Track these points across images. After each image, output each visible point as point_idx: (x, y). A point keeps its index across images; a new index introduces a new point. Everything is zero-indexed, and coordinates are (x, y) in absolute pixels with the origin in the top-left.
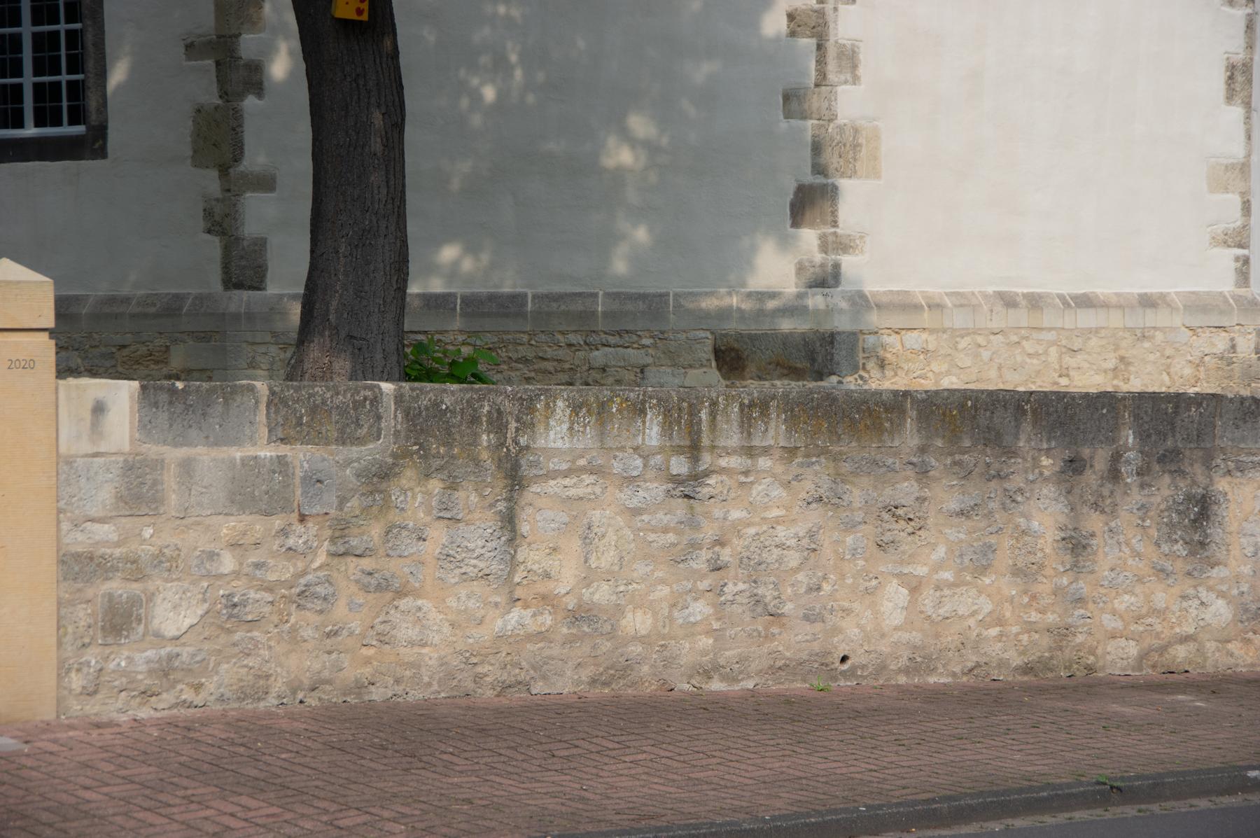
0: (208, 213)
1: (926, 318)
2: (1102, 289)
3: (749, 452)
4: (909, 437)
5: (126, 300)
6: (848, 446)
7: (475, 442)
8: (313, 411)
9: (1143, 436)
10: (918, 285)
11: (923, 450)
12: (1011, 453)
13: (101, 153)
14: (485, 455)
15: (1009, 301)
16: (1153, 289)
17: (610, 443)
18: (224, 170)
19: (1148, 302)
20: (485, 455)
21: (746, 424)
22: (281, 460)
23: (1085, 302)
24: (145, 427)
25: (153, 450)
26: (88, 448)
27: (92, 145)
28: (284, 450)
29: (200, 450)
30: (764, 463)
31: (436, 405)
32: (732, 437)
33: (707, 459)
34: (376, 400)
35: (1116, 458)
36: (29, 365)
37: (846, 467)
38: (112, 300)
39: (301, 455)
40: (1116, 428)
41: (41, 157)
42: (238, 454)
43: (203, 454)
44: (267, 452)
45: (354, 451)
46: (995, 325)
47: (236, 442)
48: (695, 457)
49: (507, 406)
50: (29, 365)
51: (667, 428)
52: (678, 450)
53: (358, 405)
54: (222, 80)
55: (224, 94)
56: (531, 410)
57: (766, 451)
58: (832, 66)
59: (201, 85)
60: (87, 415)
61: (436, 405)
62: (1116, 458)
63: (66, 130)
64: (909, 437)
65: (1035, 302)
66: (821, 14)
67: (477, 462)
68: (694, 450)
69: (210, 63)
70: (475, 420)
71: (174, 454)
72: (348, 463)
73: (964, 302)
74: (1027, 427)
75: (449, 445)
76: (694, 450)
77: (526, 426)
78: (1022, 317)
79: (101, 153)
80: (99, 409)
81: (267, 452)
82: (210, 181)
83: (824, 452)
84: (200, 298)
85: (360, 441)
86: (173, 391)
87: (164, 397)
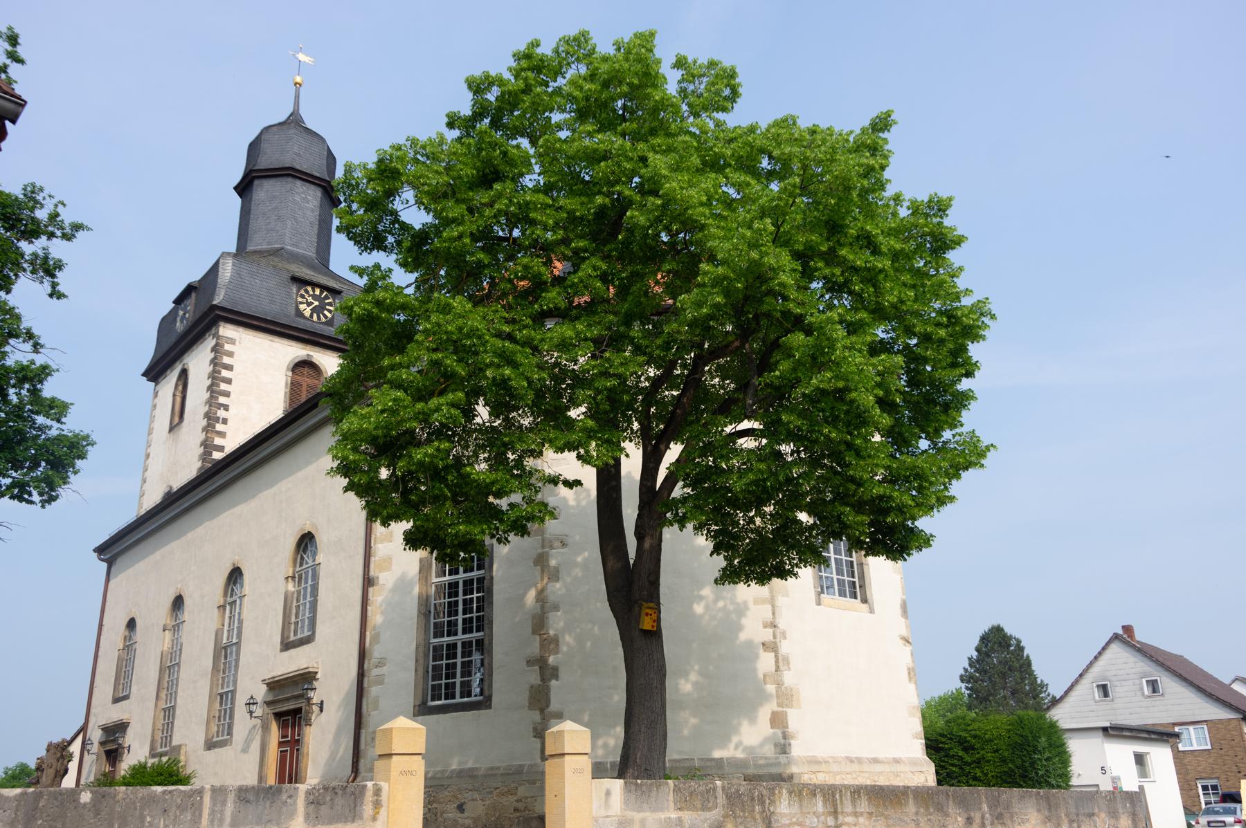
0: (535, 729)
1: (824, 767)
2: (881, 756)
3: (856, 814)
4: (911, 808)
5: (498, 768)
6: (890, 812)
7: (753, 811)
8: (691, 794)
9: (990, 807)
10: (821, 753)
11: (917, 814)
12: (947, 815)
13: (490, 707)
14: (758, 816)
15: (851, 760)
16: (897, 756)
17: (805, 810)
18: (542, 711)
19: (897, 761)
20: (758, 816)
21: (853, 801)
22: (679, 818)
23: (876, 761)
24: (626, 802)
25: (631, 814)
26: (603, 813)
27: (485, 703)
28: (681, 814)
29: (648, 814)
30: (861, 820)
31: (738, 791)
32: (849, 808)
33: (840, 817)
34: (714, 789)
35: (983, 817)
36: (581, 771)
37: (891, 822)
38: (492, 768)
39: (687, 816)
40: (980, 804)
41: (463, 710)
42: (663, 816)
43: (649, 816)
44: (674, 815)
45: (708, 814)
46: (848, 770)
47: (662, 810)
48: (836, 818)
49: (765, 792)
50: (581, 771)
51: (825, 801)
52: (830, 814)
53: (708, 791)
54: (542, 674)
55: (543, 680)
56: (774, 794)
57: (861, 814)
58: (781, 664)
59: (534, 678)
60: (603, 796)
61: (738, 791)
62: (983, 817)
63: (458, 700)
64: (911, 808)
65: (859, 761)
66: (775, 643)
67: (755, 820)
68: (835, 813)
69: (537, 668)
70: (753, 799)
71: (637, 816)
72: (706, 820)
73: (836, 761)
74: (951, 803)
75: (743, 811)
76: (835, 813)
77: (772, 802)
78: (856, 767)
79: (490, 707)
80: (608, 793)
81: (674, 815)
82: (536, 716)
83: (882, 815)
84: (531, 766)
85: (710, 809)
86: (636, 784)
87: (633, 787)
